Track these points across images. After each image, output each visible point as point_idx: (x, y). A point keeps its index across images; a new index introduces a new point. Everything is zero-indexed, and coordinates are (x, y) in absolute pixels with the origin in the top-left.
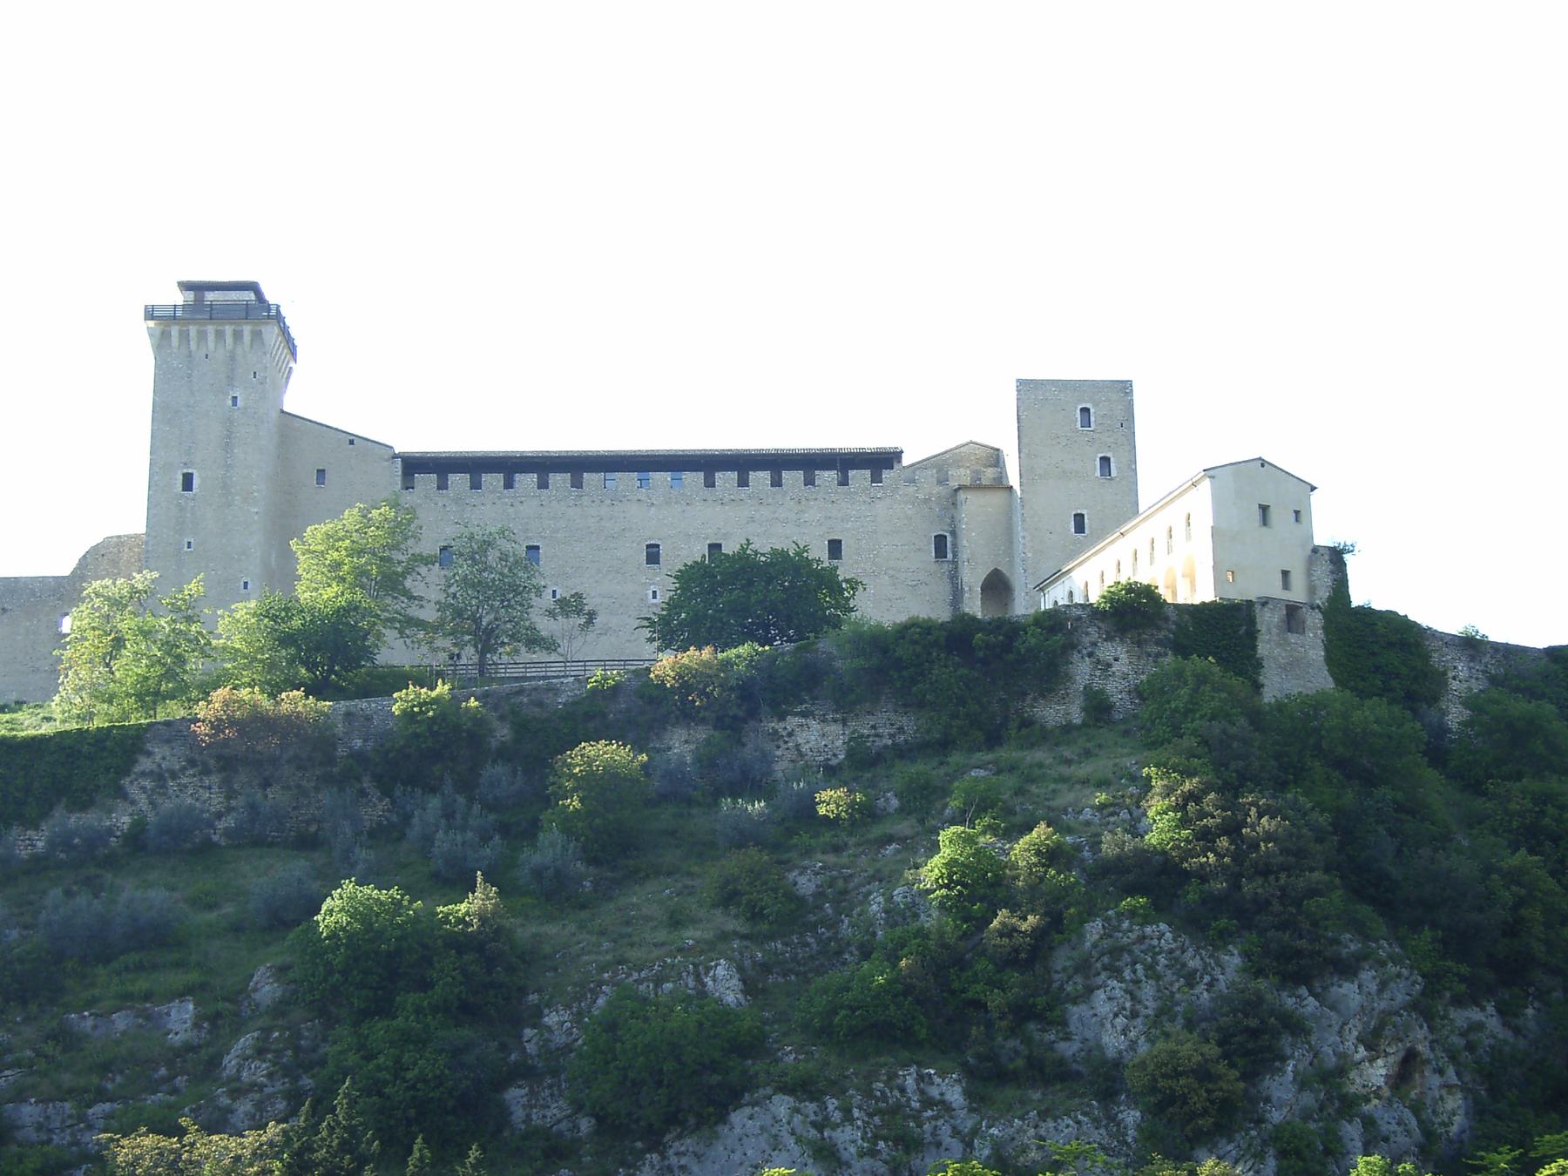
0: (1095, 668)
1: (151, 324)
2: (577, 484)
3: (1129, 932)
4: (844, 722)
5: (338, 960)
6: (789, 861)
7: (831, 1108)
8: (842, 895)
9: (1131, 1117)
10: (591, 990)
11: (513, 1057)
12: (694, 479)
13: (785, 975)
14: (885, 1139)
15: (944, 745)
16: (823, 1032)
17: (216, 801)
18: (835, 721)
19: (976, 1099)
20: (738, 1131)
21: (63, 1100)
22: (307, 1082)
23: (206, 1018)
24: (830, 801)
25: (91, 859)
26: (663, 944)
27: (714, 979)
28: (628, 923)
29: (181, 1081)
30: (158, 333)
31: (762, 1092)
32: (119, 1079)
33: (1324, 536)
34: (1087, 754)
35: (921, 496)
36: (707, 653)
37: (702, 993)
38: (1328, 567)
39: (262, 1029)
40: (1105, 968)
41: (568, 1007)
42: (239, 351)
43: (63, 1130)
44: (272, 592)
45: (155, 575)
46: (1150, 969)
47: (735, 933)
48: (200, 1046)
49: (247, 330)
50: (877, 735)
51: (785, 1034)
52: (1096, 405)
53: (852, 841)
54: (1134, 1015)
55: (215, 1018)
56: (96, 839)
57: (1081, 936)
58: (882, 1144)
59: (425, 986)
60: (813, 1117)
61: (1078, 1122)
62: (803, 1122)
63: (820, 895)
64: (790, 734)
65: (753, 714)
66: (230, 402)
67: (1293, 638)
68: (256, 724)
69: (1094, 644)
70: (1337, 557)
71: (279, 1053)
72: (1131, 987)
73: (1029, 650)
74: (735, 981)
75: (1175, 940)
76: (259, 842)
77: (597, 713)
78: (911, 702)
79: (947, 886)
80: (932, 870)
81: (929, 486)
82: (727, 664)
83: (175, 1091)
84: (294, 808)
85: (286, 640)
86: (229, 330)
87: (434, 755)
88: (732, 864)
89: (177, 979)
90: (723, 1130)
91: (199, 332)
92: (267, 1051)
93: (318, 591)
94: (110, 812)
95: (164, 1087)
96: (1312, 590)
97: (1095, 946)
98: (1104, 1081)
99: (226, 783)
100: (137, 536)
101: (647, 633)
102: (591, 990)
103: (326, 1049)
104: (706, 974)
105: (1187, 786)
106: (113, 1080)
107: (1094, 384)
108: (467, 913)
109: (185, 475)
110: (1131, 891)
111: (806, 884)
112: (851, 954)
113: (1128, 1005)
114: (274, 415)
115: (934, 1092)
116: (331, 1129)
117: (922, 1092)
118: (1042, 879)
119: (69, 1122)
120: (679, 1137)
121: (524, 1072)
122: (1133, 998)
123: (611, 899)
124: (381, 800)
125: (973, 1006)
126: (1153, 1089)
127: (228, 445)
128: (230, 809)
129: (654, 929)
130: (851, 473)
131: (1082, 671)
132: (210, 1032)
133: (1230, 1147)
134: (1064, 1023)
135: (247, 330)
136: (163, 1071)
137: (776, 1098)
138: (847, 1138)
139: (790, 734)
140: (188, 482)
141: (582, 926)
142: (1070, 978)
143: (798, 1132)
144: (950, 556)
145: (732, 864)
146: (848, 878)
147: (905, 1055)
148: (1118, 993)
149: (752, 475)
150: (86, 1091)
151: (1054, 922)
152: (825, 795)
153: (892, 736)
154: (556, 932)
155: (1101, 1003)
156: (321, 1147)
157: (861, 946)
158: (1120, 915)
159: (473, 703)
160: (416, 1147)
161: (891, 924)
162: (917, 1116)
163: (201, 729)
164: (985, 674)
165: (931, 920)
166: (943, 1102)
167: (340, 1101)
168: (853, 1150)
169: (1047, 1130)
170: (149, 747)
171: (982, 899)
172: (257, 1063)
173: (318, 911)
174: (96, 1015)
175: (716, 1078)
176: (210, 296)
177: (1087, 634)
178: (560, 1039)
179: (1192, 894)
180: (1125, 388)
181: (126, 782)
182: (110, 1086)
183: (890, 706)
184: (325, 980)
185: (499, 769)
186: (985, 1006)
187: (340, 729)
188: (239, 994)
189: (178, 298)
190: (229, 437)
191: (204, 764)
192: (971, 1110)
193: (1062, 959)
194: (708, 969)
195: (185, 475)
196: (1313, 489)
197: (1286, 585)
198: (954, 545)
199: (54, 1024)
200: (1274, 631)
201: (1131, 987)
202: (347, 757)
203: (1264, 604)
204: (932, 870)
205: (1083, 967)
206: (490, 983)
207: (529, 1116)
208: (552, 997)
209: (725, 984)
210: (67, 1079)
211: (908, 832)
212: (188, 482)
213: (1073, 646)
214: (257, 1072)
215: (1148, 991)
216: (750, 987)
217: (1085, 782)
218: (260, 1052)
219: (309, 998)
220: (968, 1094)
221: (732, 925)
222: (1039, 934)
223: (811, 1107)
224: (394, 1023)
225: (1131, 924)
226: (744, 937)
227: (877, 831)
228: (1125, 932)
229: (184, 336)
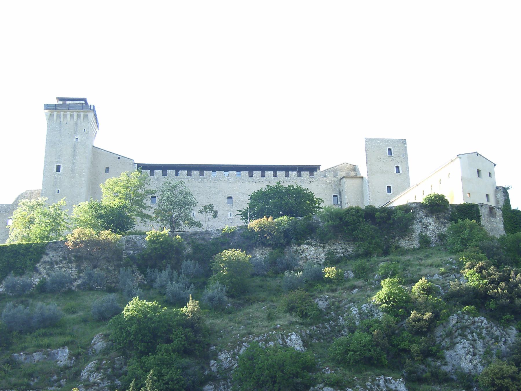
1: (47, 111)
2: (202, 174)
3: (468, 320)
4: (324, 247)
5: (133, 329)
6: (314, 295)
8: (338, 309)
11: (206, 372)
12: (245, 174)
13: (318, 340)
15: (367, 254)
16: (342, 361)
17: (74, 274)
18: (320, 247)
22: (118, 382)
23: (74, 355)
24: (329, 272)
25: (22, 294)
26: (267, 326)
28: (250, 319)
29: (63, 382)
30: (49, 114)
32: (36, 380)
33: (500, 183)
34: (428, 256)
35: (328, 181)
36: (270, 219)
37: (285, 345)
39: (98, 360)
40: (459, 335)
41: (229, 351)
42: (79, 121)
45: (46, 198)
46: (479, 334)
47: (296, 322)
48: (71, 367)
50: (337, 252)
51: (324, 363)
52: (394, 147)
53: (339, 288)
54: (474, 354)
55: (77, 356)
56: (26, 287)
57: (448, 322)
59: (169, 341)
63: (328, 308)
64: (303, 252)
65: (288, 244)
66: (75, 140)
67: (492, 219)
68: (91, 244)
69: (421, 218)
70: (505, 191)
71: (106, 370)
73: (399, 218)
74: (300, 341)
75: (488, 323)
76: (91, 289)
77: (226, 240)
78: (352, 239)
79: (386, 302)
80: (379, 297)
81: (331, 177)
82: (278, 224)
83: (60, 386)
84: (106, 277)
85: (100, 216)
86: (75, 114)
87: (161, 256)
88: (292, 296)
89: (61, 339)
91: (64, 115)
92: (101, 369)
93: (110, 201)
94: (31, 277)
95: (56, 384)
96: (497, 202)
97: (454, 326)
99: (78, 266)
102: (238, 345)
103: (125, 368)
104: (287, 338)
105: (480, 264)
106: (33, 381)
107: (393, 140)
108: (186, 312)
110: (465, 304)
111: (322, 304)
112: (345, 331)
113: (472, 350)
114: (91, 147)
115: (392, 387)
117: (387, 387)
118: (427, 299)
122: (473, 347)
123: (240, 310)
127: (74, 155)
128: (80, 277)
131: (417, 228)
132: (75, 361)
134: (444, 358)
135: (82, 114)
136: (55, 377)
139: (303, 252)
140: (58, 169)
141: (231, 320)
142: (444, 339)
145: (292, 296)
147: (377, 371)
148: (467, 345)
149: (266, 173)
150: (22, 385)
151: (436, 316)
152: (327, 270)
153: (343, 253)
154: (220, 322)
157: (349, 328)
159: (178, 236)
161: (362, 319)
163: (70, 244)
164: (375, 231)
165: (381, 316)
170: (47, 252)
171: (402, 307)
172: (97, 374)
174: (26, 354)
175: (299, 380)
176: (68, 102)
178: (226, 365)
180: (404, 142)
181: (38, 265)
182: (32, 383)
183: (342, 241)
184: (126, 339)
186: (410, 351)
187: (124, 247)
188: (88, 346)
189: (55, 102)
190: (74, 152)
191: (70, 259)
193: (439, 331)
196: (495, 165)
197: (488, 200)
198: (341, 199)
199: (8, 357)
200: (486, 216)
201: (472, 342)
202: (127, 257)
203: (482, 206)
204: (379, 297)
205: (450, 335)
206: (196, 342)
208: (222, 348)
209: (295, 342)
210: (13, 380)
211: (360, 285)
212: (58, 169)
213: (413, 218)
215: (480, 344)
216: (306, 344)
217: (431, 266)
218: (98, 369)
219: (118, 347)
221: (294, 320)
222: (431, 321)
224: (157, 356)
225: (469, 317)
227: (348, 284)
229: (59, 116)
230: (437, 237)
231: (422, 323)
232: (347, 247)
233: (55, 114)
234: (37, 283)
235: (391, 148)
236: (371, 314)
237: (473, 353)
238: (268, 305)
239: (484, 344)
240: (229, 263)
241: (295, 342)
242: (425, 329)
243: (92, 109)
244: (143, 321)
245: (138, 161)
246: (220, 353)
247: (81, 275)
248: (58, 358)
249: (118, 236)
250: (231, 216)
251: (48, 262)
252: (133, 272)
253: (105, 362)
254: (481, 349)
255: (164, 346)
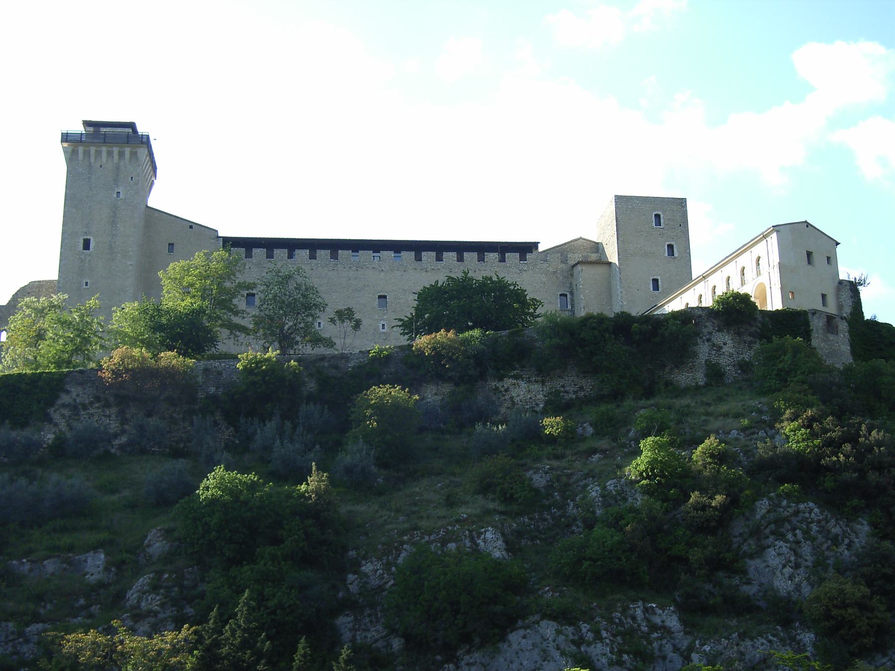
0: (712, 349)
1: (66, 145)
2: (334, 256)
3: (787, 508)
6: (525, 465)
7: (584, 630)
9: (808, 638)
10: (396, 549)
11: (340, 595)
12: (408, 256)
13: (532, 540)
14: (628, 653)
15: (617, 396)
17: (114, 426)
18: (536, 382)
19: (689, 626)
20: (515, 646)
21: (6, 620)
22: (189, 610)
24: (552, 424)
26: (444, 517)
27: (485, 541)
28: (415, 504)
29: (95, 609)
30: (70, 150)
31: (532, 619)
32: (49, 606)
34: (720, 399)
35: (551, 270)
36: (451, 334)
38: (849, 293)
39: (156, 572)
40: (772, 533)
41: (379, 559)
42: (122, 163)
43: (6, 643)
44: (148, 299)
45: (66, 296)
46: (806, 532)
47: (495, 510)
48: (109, 584)
49: (127, 151)
52: (664, 212)
53: (568, 452)
54: (797, 566)
55: (120, 565)
57: (753, 511)
58: (625, 657)
59: (277, 541)
60: (571, 637)
61: (770, 641)
62: (566, 640)
63: (550, 487)
65: (482, 376)
66: (115, 195)
67: (831, 337)
68: (142, 374)
69: (710, 333)
70: (853, 288)
72: (794, 546)
74: (500, 542)
75: (821, 513)
76: (143, 452)
77: (377, 369)
79: (648, 477)
80: (642, 462)
81: (556, 264)
82: (465, 342)
84: (168, 432)
86: (116, 150)
87: (262, 397)
89: (92, 537)
90: (504, 646)
91: (96, 151)
93: (175, 301)
94: (40, 431)
95: (83, 613)
96: (840, 307)
97: (763, 517)
98: (783, 613)
99: (121, 412)
100: (51, 282)
101: (400, 330)
102: (396, 549)
103: (202, 587)
104: (479, 537)
106: (45, 607)
108: (306, 491)
109: (84, 240)
111: (539, 480)
112: (577, 526)
113: (792, 558)
114: (143, 207)
115: (657, 620)
116: (233, 632)
117: (648, 620)
118: (718, 471)
119: (11, 637)
120: (468, 652)
121: (350, 605)
122: (796, 554)
124: (228, 429)
125: (677, 557)
126: (828, 617)
128: (123, 432)
129: (436, 507)
130: (507, 255)
131: (703, 351)
133: (885, 660)
134: (745, 572)
135: (127, 151)
137: (544, 623)
138: (600, 652)
139: (507, 390)
140: (87, 245)
142: (745, 540)
143: (562, 647)
144: (569, 307)
146: (569, 476)
148: (785, 550)
149: (445, 254)
151: (733, 501)
152: (547, 421)
153: (575, 392)
155: (772, 558)
156: (225, 646)
158: (779, 496)
160: (300, 646)
161: (606, 505)
162: (646, 636)
165: (639, 500)
166: (664, 627)
167: (241, 610)
168: (604, 660)
169: (746, 647)
170: (68, 387)
171: (675, 486)
172: (153, 596)
173: (198, 488)
175: (499, 608)
176: (103, 130)
177: (706, 327)
178: (374, 582)
179: (828, 482)
180: (682, 203)
181: (51, 411)
182: (42, 611)
185: (311, 406)
189: (80, 129)
192: (686, 633)
193: (739, 527)
194: (479, 534)
195: (84, 240)
196: (838, 244)
197: (824, 303)
198: (572, 300)
201: (794, 546)
205: (756, 532)
206: (322, 542)
207: (354, 637)
209: (491, 542)
212: (87, 245)
214: (153, 602)
215: (806, 549)
216: (510, 547)
217: (726, 415)
218: (155, 588)
220: (683, 621)
221: (491, 506)
222: (724, 508)
223: (570, 629)
226: (502, 513)
227: (583, 446)
228: (785, 508)
229: (87, 154)
230: (737, 367)
231: (709, 512)
232: (583, 382)
233: (81, 149)
234: (50, 442)
235: (659, 213)
236: (621, 496)
237: (795, 563)
238: (447, 481)
239: (814, 549)
240: (380, 409)
241: (491, 542)
242: (713, 524)
243: (145, 141)
244: (232, 504)
245: (226, 231)
246: (363, 562)
247: (126, 427)
248: (86, 570)
249: (190, 362)
250: (383, 328)
251: (70, 404)
252: (215, 423)
253: (166, 576)
254: (809, 558)
255: (269, 549)
